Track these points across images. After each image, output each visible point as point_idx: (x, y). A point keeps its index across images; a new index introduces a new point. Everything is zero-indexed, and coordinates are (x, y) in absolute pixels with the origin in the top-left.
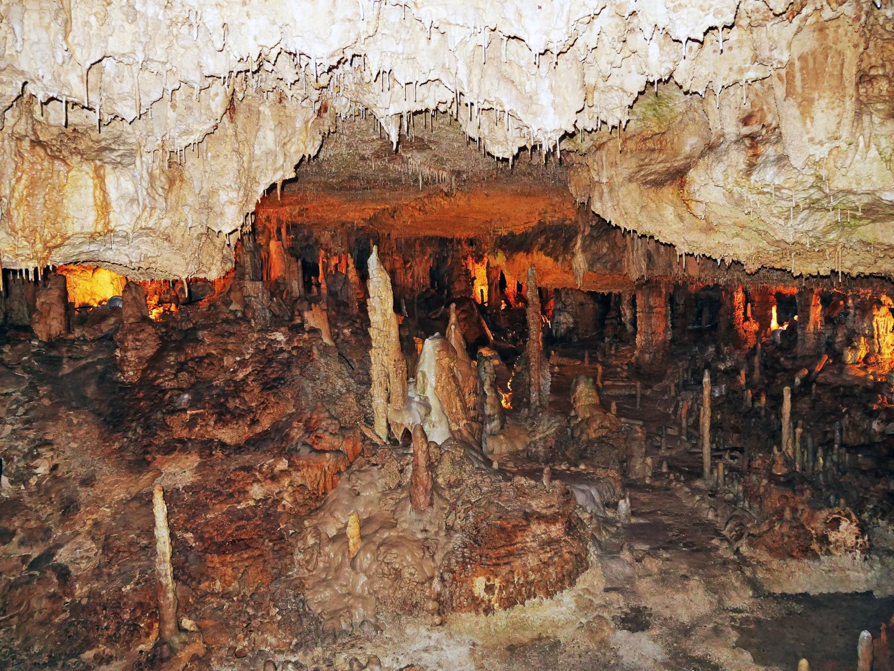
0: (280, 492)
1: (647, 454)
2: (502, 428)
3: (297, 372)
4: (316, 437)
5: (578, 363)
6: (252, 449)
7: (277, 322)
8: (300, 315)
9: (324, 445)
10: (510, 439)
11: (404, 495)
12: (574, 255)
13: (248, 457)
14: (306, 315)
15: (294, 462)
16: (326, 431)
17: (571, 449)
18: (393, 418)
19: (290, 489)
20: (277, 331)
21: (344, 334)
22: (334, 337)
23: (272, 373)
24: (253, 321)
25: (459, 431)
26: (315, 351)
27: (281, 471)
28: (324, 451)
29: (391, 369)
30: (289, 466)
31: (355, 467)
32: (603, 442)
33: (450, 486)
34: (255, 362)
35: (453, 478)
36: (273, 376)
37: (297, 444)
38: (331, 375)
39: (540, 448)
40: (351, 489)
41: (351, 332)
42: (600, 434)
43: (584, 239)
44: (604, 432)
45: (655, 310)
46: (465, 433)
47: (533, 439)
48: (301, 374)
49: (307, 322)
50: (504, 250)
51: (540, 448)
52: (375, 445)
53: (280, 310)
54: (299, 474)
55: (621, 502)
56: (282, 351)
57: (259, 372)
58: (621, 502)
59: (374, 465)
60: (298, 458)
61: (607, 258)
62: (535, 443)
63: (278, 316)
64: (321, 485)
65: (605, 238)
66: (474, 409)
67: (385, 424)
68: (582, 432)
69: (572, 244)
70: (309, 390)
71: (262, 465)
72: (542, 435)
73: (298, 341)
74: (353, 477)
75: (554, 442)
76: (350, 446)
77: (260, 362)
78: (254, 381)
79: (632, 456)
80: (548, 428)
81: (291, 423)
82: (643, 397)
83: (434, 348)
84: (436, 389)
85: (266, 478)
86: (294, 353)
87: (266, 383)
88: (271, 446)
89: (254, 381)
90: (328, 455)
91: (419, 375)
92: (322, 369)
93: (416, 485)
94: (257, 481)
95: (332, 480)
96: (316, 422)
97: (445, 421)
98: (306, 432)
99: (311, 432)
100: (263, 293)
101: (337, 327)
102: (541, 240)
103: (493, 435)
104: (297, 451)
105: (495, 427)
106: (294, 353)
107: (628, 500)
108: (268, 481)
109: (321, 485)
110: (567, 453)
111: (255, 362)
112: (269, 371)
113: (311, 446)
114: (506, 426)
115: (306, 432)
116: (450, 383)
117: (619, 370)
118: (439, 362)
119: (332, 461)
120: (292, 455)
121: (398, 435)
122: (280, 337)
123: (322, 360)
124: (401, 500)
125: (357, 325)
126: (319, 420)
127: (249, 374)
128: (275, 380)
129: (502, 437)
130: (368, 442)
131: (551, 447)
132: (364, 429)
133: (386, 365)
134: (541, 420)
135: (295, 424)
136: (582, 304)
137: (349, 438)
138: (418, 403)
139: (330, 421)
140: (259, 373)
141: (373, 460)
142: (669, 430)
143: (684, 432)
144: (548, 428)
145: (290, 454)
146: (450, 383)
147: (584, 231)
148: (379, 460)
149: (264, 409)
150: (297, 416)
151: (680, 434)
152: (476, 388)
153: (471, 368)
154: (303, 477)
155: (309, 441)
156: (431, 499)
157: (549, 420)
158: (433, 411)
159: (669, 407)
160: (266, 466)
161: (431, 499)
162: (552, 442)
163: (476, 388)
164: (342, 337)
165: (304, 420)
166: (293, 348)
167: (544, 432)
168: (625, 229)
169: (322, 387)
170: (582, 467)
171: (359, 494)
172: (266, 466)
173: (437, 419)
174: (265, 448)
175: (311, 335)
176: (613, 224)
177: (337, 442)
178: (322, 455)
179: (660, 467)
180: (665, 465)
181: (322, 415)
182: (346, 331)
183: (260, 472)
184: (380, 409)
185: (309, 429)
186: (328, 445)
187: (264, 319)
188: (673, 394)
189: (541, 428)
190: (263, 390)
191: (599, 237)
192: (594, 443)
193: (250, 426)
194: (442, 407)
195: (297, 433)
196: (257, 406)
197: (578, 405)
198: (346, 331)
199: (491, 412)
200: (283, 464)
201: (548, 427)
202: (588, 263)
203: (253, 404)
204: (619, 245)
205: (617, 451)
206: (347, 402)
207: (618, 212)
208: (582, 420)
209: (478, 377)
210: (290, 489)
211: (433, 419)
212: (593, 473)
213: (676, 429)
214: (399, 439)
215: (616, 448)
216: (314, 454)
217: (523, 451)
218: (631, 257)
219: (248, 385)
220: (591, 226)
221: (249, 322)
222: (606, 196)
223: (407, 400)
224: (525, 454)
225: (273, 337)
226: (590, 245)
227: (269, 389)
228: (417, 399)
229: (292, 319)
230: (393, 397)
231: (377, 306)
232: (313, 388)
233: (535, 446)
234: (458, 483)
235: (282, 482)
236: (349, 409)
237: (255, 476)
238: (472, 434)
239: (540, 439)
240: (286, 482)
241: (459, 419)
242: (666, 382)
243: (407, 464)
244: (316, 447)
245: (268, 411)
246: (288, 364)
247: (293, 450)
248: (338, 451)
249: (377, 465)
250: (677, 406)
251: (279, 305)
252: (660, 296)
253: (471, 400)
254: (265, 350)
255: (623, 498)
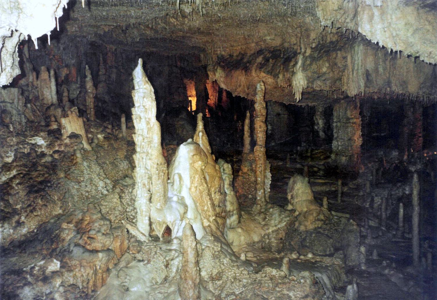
0: (51, 293)
1: (361, 244)
2: (239, 222)
3: (62, 175)
4: (89, 238)
5: (281, 164)
6: (18, 251)
7: (34, 128)
8: (56, 121)
9: (97, 245)
10: (247, 231)
11: (172, 289)
12: (293, 73)
13: (14, 259)
14: (63, 121)
15: (67, 263)
16: (99, 231)
17: (296, 239)
18: (156, 217)
19: (61, 289)
20: (37, 136)
21: (98, 139)
22: (90, 141)
23: (37, 176)
24: (11, 126)
25: (209, 226)
26: (79, 155)
27: (53, 272)
28: (95, 251)
29: (154, 171)
30: (61, 267)
31: (122, 264)
32: (319, 232)
33: (212, 279)
34: (21, 166)
35: (215, 272)
36: (40, 179)
37: (69, 245)
38: (92, 178)
39: (273, 240)
40: (120, 285)
41: (104, 138)
42: (316, 226)
43: (305, 58)
44: (320, 224)
45: (351, 121)
46: (214, 228)
47: (267, 232)
48: (66, 177)
49: (64, 128)
50: (223, 68)
51: (273, 240)
52: (139, 242)
53: (34, 115)
54: (71, 274)
55: (349, 287)
56: (43, 155)
57: (25, 175)
58: (349, 287)
59: (139, 261)
60: (70, 259)
61: (327, 76)
62: (268, 235)
63: (32, 122)
64: (91, 283)
65: (325, 59)
66: (219, 206)
67: (147, 222)
68: (300, 224)
69: (292, 64)
70: (74, 192)
71: (33, 268)
72: (275, 228)
73: (60, 145)
74: (121, 273)
75: (284, 235)
76: (118, 244)
77: (25, 165)
78: (19, 184)
79: (348, 245)
80: (280, 222)
81: (60, 224)
82: (343, 193)
83: (188, 152)
84: (190, 189)
85: (37, 280)
86: (56, 156)
87: (33, 186)
88: (39, 247)
89: (19, 184)
90: (100, 255)
91: (176, 178)
92: (85, 172)
93: (186, 280)
94: (28, 284)
95: (103, 279)
96: (89, 224)
97: (199, 217)
98: (78, 233)
99: (84, 233)
100: (19, 99)
101: (91, 133)
102: (260, 59)
103: (232, 228)
104: (70, 252)
105: (234, 221)
106: (56, 156)
107: (355, 286)
108: (40, 283)
109: (91, 283)
110: (292, 243)
111: (21, 166)
112: (34, 174)
113: (84, 247)
114: (242, 220)
115: (78, 233)
116: (202, 184)
117: (315, 169)
118: (192, 165)
119: (104, 260)
120: (64, 256)
121: (159, 232)
122: (40, 141)
123: (85, 164)
124: (169, 295)
125: (109, 131)
126: (92, 222)
127: (15, 177)
128: (41, 183)
129: (240, 230)
130: (133, 240)
131: (281, 239)
132: (129, 227)
133: (149, 168)
134: (272, 214)
135: (64, 225)
136: (279, 114)
137: (117, 236)
138: (177, 202)
139: (102, 222)
140: (24, 177)
141: (139, 256)
142: (370, 222)
143: (384, 224)
144: (280, 222)
145: (63, 255)
146: (202, 184)
147: (305, 52)
148: (145, 257)
149: (31, 211)
150: (66, 216)
151: (380, 224)
152: (220, 188)
153: (216, 170)
154: (75, 276)
155: (81, 242)
156: (199, 292)
157: (280, 215)
158: (189, 210)
159: (364, 201)
160: (37, 268)
161: (199, 292)
162: (282, 234)
163: (220, 188)
164: (96, 141)
165: (74, 221)
166: (55, 152)
167: (276, 226)
168: (392, 50)
169: (87, 189)
170: (310, 256)
171: (127, 290)
172: (37, 268)
173: (193, 217)
174: (33, 250)
175: (73, 140)
176: (381, 44)
177: (108, 242)
178: (95, 255)
179: (371, 254)
180: (375, 253)
181: (95, 217)
182: (99, 136)
183: (32, 275)
184: (144, 208)
185: (80, 230)
186: (100, 245)
187: (20, 124)
188: (368, 190)
189: (273, 222)
190: (30, 192)
191: (320, 58)
192: (311, 234)
193: (15, 228)
194: (196, 206)
195: (68, 233)
196: (22, 208)
197: (296, 200)
198: (99, 136)
199: (231, 208)
200: (55, 265)
201: (277, 222)
202: (308, 80)
203: (18, 207)
204: (339, 65)
205: (331, 240)
206: (112, 202)
207: (387, 34)
208: (300, 214)
209: (221, 178)
210: (61, 289)
211: (189, 217)
212: (321, 261)
213: (377, 221)
214: (160, 236)
215: (331, 238)
216: (87, 254)
217: (258, 242)
218: (351, 76)
219: (13, 188)
220: (312, 48)
221: (8, 127)
222: (377, 18)
223: (166, 199)
224: (260, 244)
225: (33, 142)
226: (311, 64)
227: (37, 192)
228: (175, 199)
229: (48, 125)
230: (155, 198)
231: (142, 115)
232: (78, 190)
233: (268, 238)
234: (219, 276)
235: (54, 283)
236: (114, 209)
237: (25, 278)
238: (218, 228)
239: (273, 232)
240: (58, 282)
241: (209, 216)
242: (360, 181)
243: (172, 260)
244: (88, 247)
245: (35, 214)
246: (53, 167)
247: (65, 250)
248: (108, 250)
249: (143, 261)
250: (372, 201)
251: (34, 111)
252: (355, 108)
253: (217, 197)
254: (29, 154)
255: (350, 283)
